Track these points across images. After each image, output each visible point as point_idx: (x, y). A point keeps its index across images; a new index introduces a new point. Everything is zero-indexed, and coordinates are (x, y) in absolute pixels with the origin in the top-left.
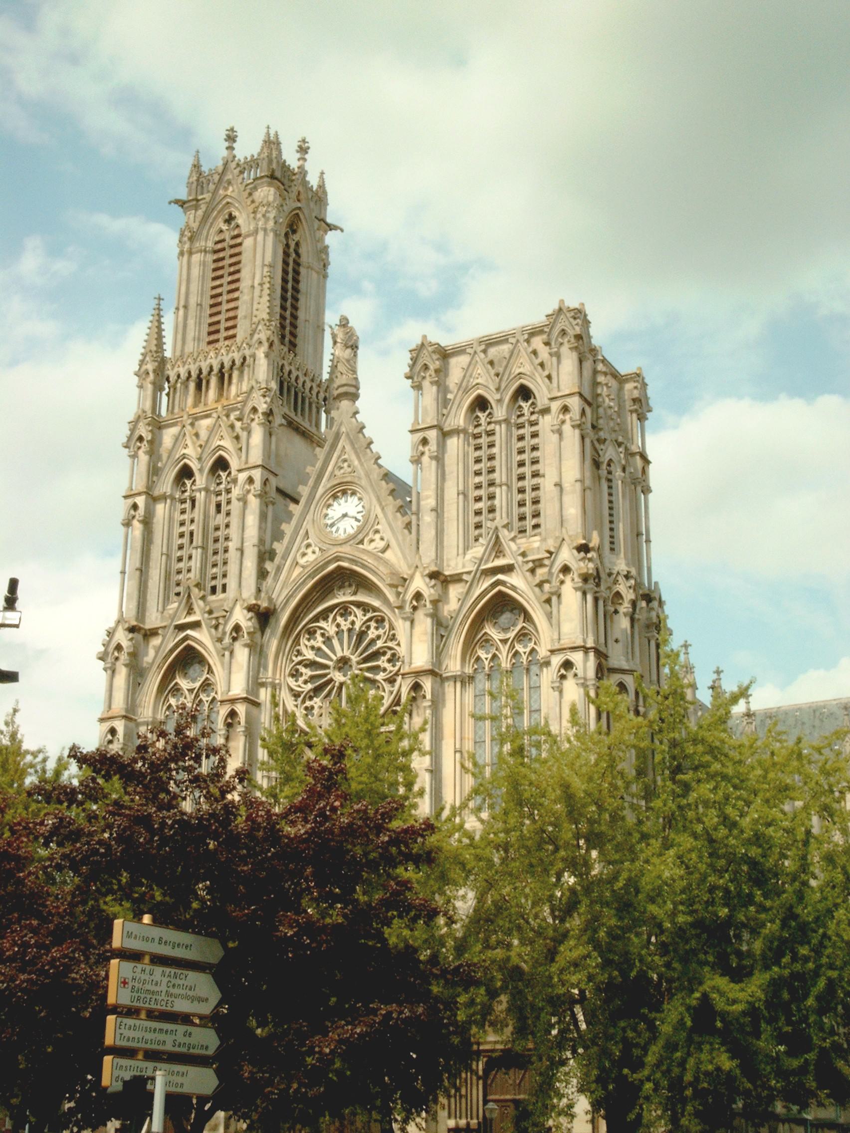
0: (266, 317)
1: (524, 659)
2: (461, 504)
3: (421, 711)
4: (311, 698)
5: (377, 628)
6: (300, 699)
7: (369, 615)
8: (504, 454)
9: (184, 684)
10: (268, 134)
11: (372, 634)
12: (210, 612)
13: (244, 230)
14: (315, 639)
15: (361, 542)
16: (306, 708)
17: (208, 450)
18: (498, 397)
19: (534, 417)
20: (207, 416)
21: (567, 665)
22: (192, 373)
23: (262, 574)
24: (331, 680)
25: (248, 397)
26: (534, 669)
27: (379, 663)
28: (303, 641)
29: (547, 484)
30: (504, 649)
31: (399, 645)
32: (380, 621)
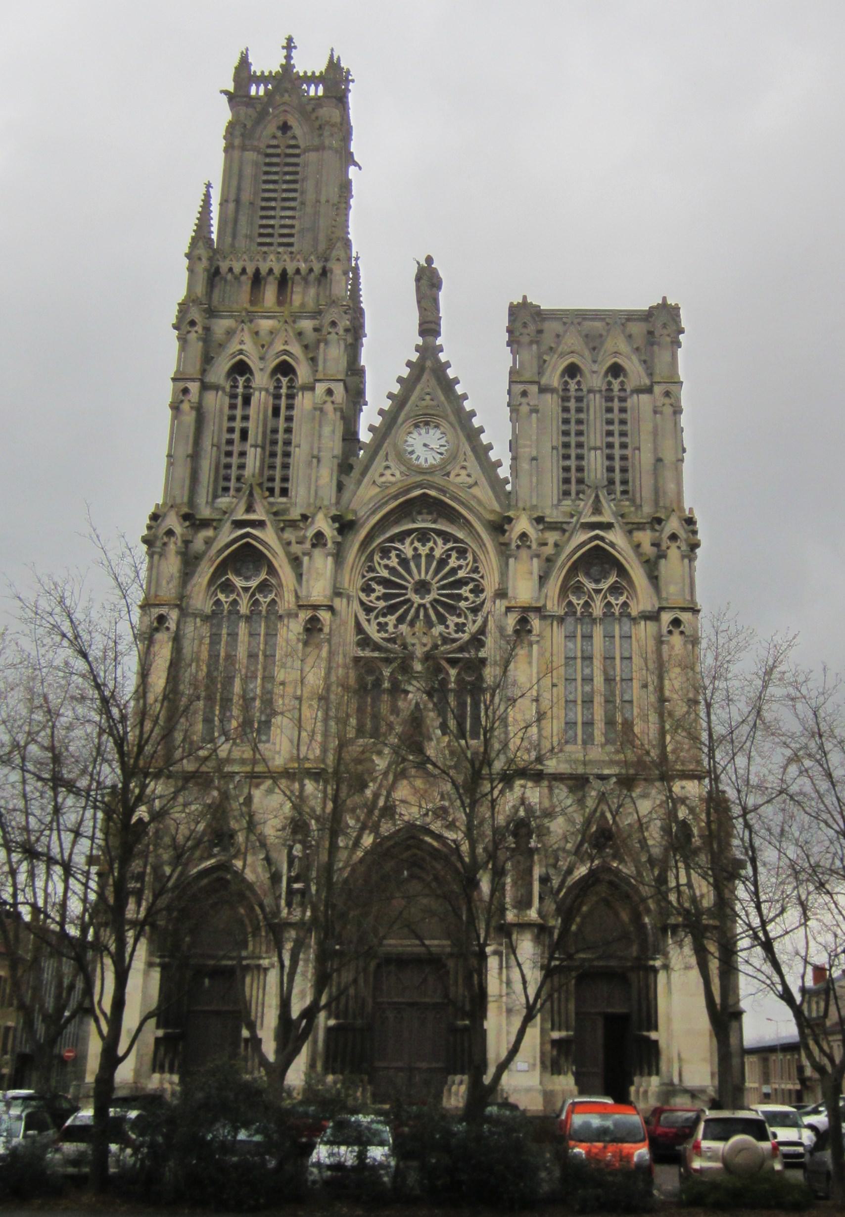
1: (263, 608)
7: (450, 545)
10: (332, 56)
11: (453, 562)
16: (379, 624)
21: (676, 622)
24: (408, 601)
28: (377, 558)
29: (300, 454)
30: (598, 598)
31: (482, 577)
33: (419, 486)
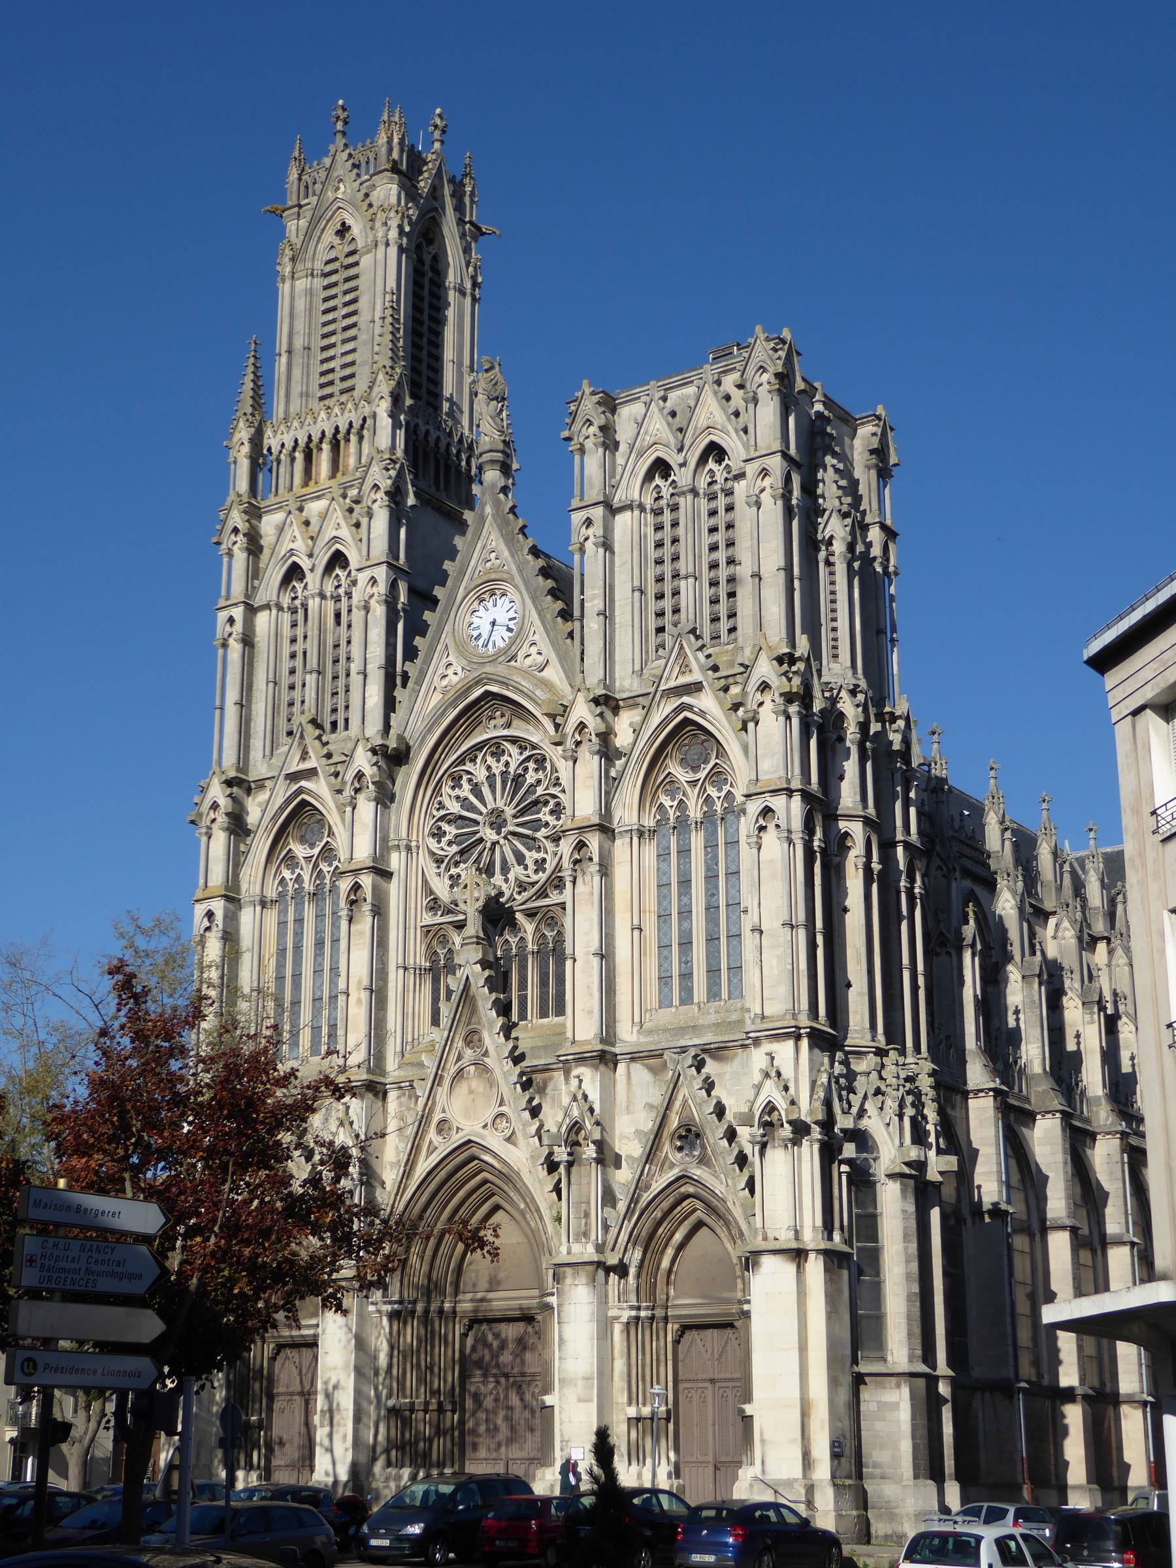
0: (389, 363)
2: (637, 605)
3: (588, 878)
4: (457, 864)
5: (536, 770)
6: (443, 866)
7: (527, 754)
8: (690, 535)
9: (300, 851)
11: (531, 777)
12: (329, 756)
13: (360, 244)
14: (460, 786)
15: (514, 658)
16: (451, 877)
17: (321, 542)
18: (680, 459)
19: (730, 484)
20: (318, 498)
21: (767, 811)
22: (327, 434)
23: (390, 704)
24: (481, 840)
25: (367, 472)
26: (730, 817)
27: (455, 831)
28: (446, 789)
30: (693, 793)
32: (541, 762)
33: (478, 682)
